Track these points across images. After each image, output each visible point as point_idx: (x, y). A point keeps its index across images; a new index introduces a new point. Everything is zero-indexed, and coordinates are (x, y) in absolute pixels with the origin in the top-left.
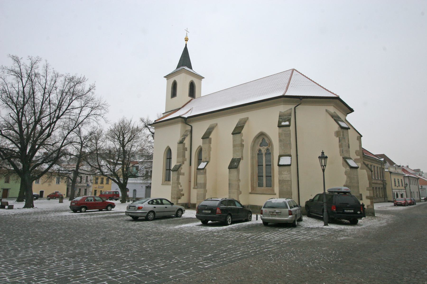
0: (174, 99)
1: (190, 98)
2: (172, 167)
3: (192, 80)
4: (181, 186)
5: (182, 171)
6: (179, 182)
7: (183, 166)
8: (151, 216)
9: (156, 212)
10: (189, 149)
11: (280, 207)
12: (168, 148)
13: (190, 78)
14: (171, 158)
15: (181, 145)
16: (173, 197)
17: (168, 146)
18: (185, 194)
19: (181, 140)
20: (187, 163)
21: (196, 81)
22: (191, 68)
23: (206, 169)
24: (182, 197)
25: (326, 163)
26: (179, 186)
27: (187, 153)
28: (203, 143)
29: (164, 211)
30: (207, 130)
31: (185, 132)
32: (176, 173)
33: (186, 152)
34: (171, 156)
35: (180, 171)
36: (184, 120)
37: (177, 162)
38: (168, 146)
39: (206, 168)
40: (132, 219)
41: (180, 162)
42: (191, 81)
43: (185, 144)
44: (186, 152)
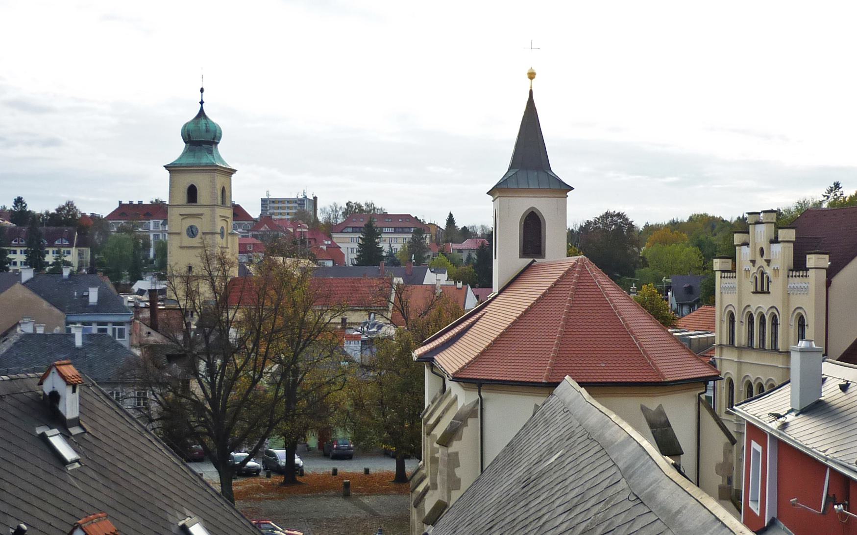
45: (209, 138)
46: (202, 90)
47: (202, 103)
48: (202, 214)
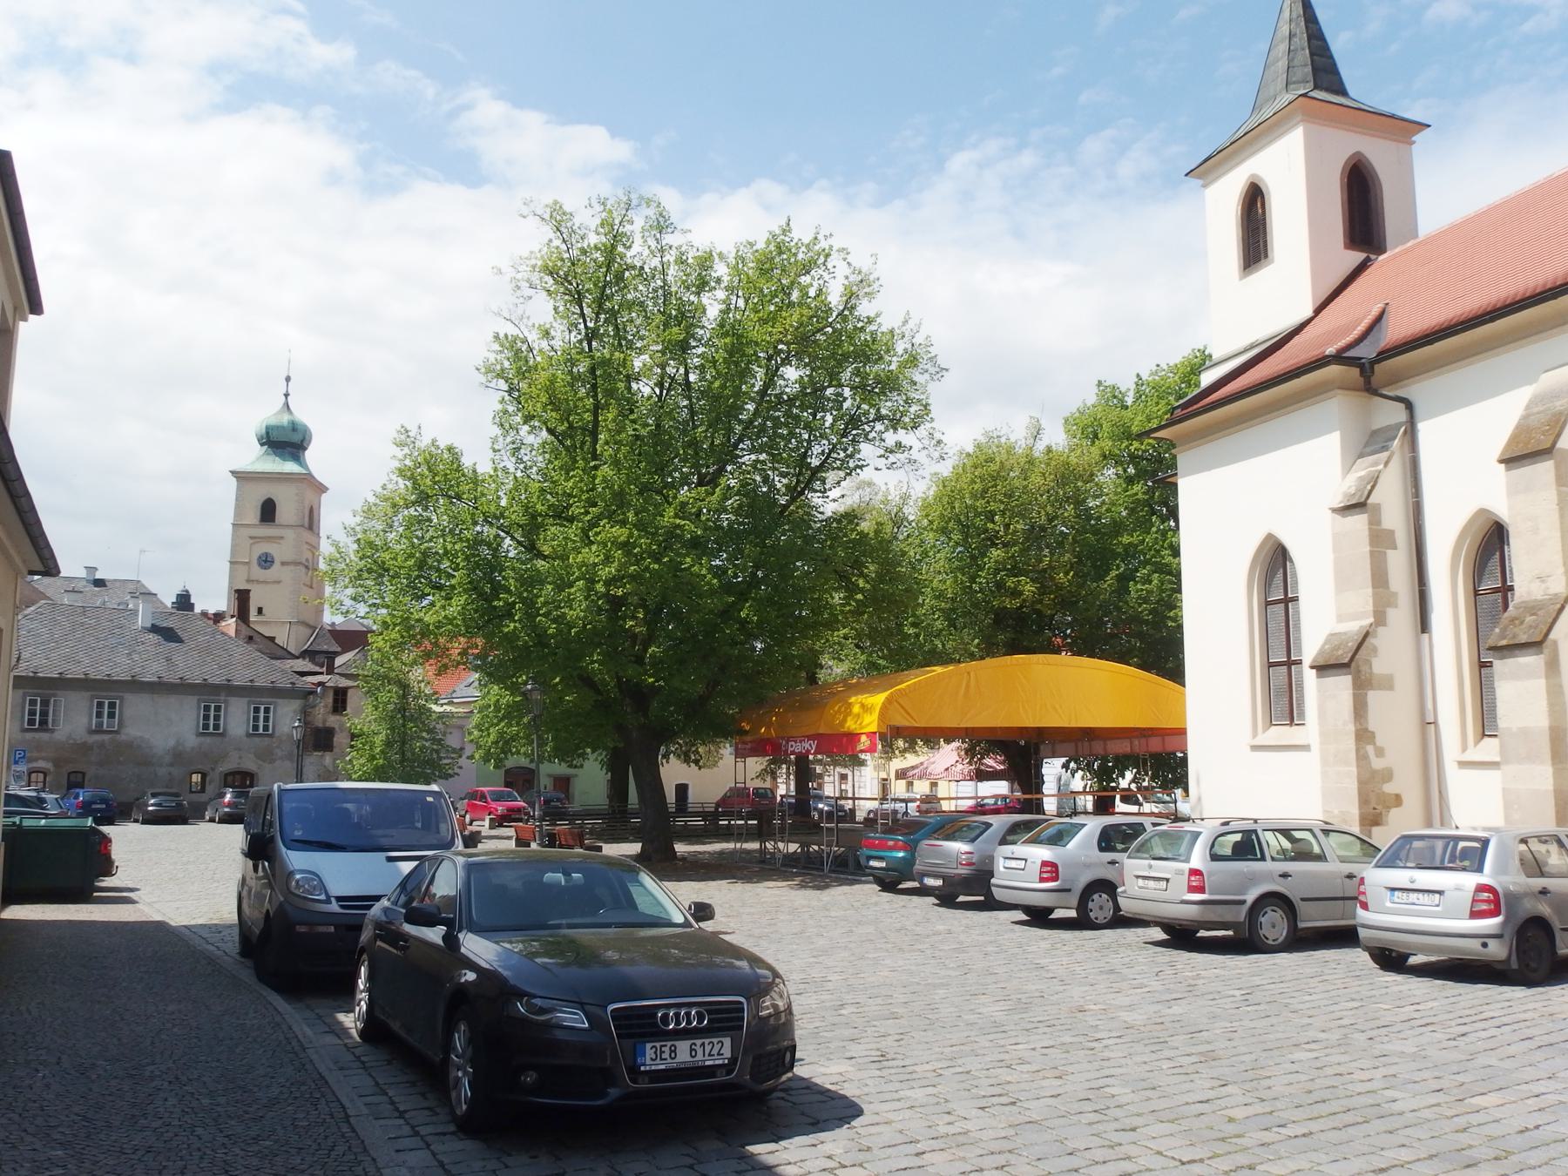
0: (1263, 275)
1: (1357, 257)
2: (1311, 646)
3: (1358, 154)
4: (1380, 752)
5: (1379, 666)
6: (1366, 730)
7: (1382, 639)
8: (1273, 925)
9: (1303, 899)
10: (1403, 537)
11: (1209, 926)
12: (1271, 542)
13: (1346, 144)
14: (1295, 599)
15: (1359, 521)
16: (1336, 812)
17: (1270, 537)
18: (1404, 797)
19: (1352, 491)
20: (1402, 615)
21: (1379, 155)
22: (1343, 92)
23: (1555, 643)
24: (1394, 815)
25: (1429, 705)
26: (1370, 749)
27: (1398, 563)
28: (1513, 491)
29: (1341, 895)
30: (1528, 407)
31: (1365, 447)
32: (1342, 684)
33: (1390, 553)
34: (1296, 583)
35: (1364, 668)
36: (1355, 371)
37: (1340, 619)
38: (1270, 537)
39: (1552, 636)
40: (1165, 937)
41: (1355, 617)
42: (1354, 154)
43: (1377, 507)
44: (1390, 553)
45: (296, 438)
46: (288, 379)
47: (287, 395)
48: (282, 538)
